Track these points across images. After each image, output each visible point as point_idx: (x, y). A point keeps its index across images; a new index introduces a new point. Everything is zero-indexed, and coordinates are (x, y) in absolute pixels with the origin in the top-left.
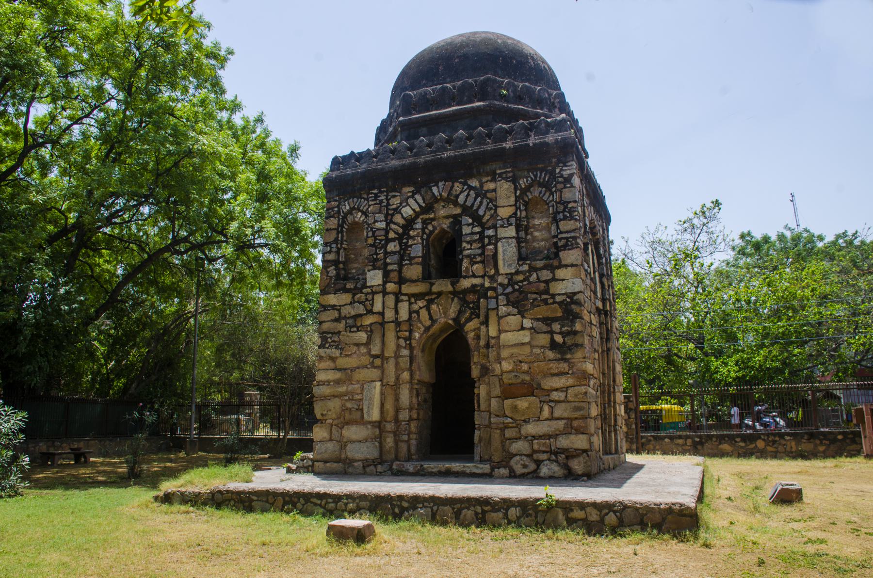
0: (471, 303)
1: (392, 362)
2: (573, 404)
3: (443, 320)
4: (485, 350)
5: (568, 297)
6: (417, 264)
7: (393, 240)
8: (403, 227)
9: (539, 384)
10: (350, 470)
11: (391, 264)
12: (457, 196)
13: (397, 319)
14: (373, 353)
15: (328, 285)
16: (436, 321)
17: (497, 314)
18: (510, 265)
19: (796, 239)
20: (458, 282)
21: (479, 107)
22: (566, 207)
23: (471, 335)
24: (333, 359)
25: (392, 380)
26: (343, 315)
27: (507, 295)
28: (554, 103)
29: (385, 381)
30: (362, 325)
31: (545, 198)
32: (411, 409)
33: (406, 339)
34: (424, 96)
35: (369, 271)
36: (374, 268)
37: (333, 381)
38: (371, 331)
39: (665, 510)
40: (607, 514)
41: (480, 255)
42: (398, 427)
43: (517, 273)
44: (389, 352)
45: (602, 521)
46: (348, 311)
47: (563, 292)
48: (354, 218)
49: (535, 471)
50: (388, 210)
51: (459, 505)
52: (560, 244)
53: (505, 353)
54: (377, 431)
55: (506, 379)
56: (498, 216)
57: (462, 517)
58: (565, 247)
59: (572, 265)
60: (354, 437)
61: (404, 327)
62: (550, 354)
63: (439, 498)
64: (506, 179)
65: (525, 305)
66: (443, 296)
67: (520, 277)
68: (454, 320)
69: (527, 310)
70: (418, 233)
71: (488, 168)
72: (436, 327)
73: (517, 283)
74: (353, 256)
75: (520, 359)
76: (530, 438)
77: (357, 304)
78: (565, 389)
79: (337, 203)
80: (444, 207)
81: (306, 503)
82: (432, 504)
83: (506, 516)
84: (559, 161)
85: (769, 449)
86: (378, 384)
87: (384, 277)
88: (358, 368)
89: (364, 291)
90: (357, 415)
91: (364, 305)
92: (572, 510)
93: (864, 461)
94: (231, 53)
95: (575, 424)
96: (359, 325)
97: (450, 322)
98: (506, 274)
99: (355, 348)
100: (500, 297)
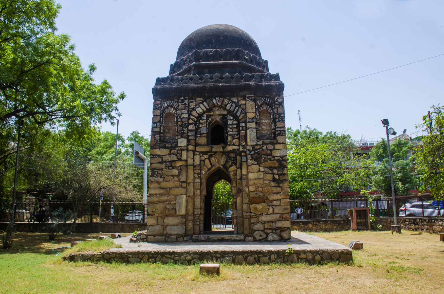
0: (232, 158)
1: (191, 185)
2: (283, 207)
3: (217, 165)
4: (240, 181)
6: (204, 137)
7: (192, 124)
8: (197, 118)
9: (267, 198)
10: (169, 240)
11: (191, 136)
12: (226, 105)
13: (194, 163)
14: (182, 180)
15: (155, 144)
16: (214, 165)
17: (247, 164)
18: (253, 141)
19: (311, 133)
20: (226, 147)
21: (236, 63)
22: (280, 116)
23: (232, 173)
24: (158, 183)
25: (192, 195)
26: (164, 160)
27: (252, 155)
28: (264, 65)
29: (188, 195)
31: (269, 111)
32: (201, 209)
33: (198, 174)
34: (206, 53)
35: (179, 138)
36: (182, 137)
37: (159, 194)
38: (181, 169)
39: (341, 252)
40: (316, 255)
41: (237, 135)
42: (194, 218)
43: (257, 145)
44: (190, 180)
45: (314, 258)
46: (167, 158)
47: (279, 155)
48: (170, 111)
49: (266, 238)
50: (189, 108)
51: (246, 255)
52: (277, 133)
53: (251, 183)
54: (184, 220)
55: (251, 195)
56: (247, 117)
57: (248, 260)
58: (279, 135)
60: (171, 223)
61: (198, 168)
62: (273, 184)
63: (236, 252)
64: (251, 100)
65: (260, 160)
66: (217, 154)
67: (258, 147)
68: (223, 165)
69: (261, 163)
70: (205, 122)
71: (242, 94)
72: (214, 168)
73: (256, 150)
74: (167, 130)
75: (258, 185)
76: (263, 223)
77: (172, 155)
78: (280, 200)
79: (160, 102)
80: (218, 110)
81: (162, 257)
82: (232, 255)
83: (270, 259)
84: (277, 94)
85: (314, 228)
86: (185, 196)
87: (187, 142)
88: (173, 188)
89: (176, 148)
90: (173, 212)
92: (300, 254)
93: (353, 232)
94: (59, 7)
95: (284, 216)
96: (174, 165)
97: (221, 167)
99: (172, 178)
100: (248, 156)
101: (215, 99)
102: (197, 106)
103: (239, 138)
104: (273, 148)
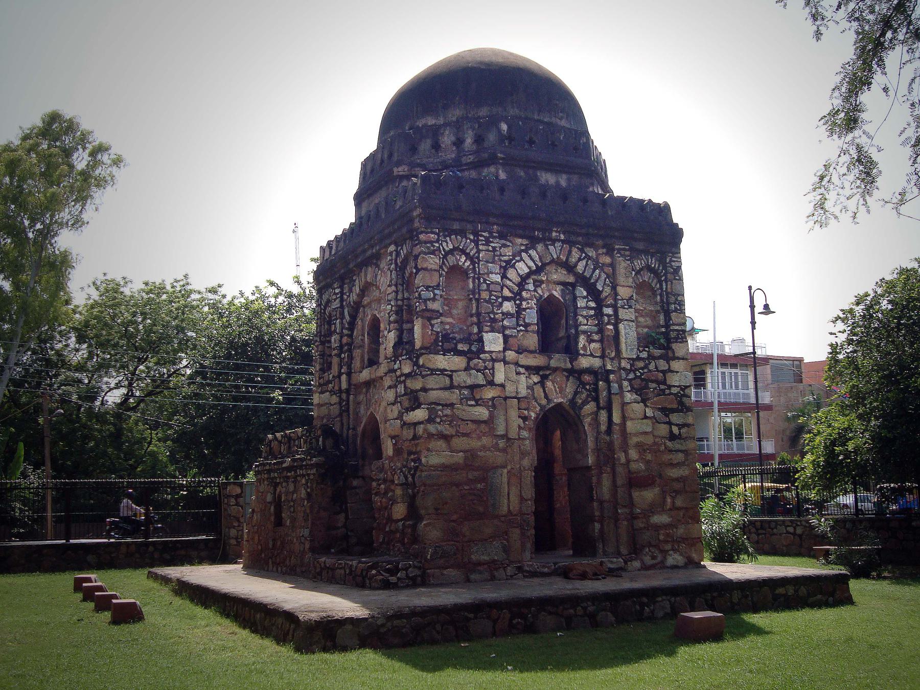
5: (682, 389)
6: (533, 332)
20: (576, 359)
27: (630, 381)
30: (481, 399)
38: (494, 406)
41: (597, 333)
43: (639, 358)
46: (462, 378)
65: (647, 393)
91: (483, 374)
98: (629, 359)
101: (553, 245)
103: (601, 341)
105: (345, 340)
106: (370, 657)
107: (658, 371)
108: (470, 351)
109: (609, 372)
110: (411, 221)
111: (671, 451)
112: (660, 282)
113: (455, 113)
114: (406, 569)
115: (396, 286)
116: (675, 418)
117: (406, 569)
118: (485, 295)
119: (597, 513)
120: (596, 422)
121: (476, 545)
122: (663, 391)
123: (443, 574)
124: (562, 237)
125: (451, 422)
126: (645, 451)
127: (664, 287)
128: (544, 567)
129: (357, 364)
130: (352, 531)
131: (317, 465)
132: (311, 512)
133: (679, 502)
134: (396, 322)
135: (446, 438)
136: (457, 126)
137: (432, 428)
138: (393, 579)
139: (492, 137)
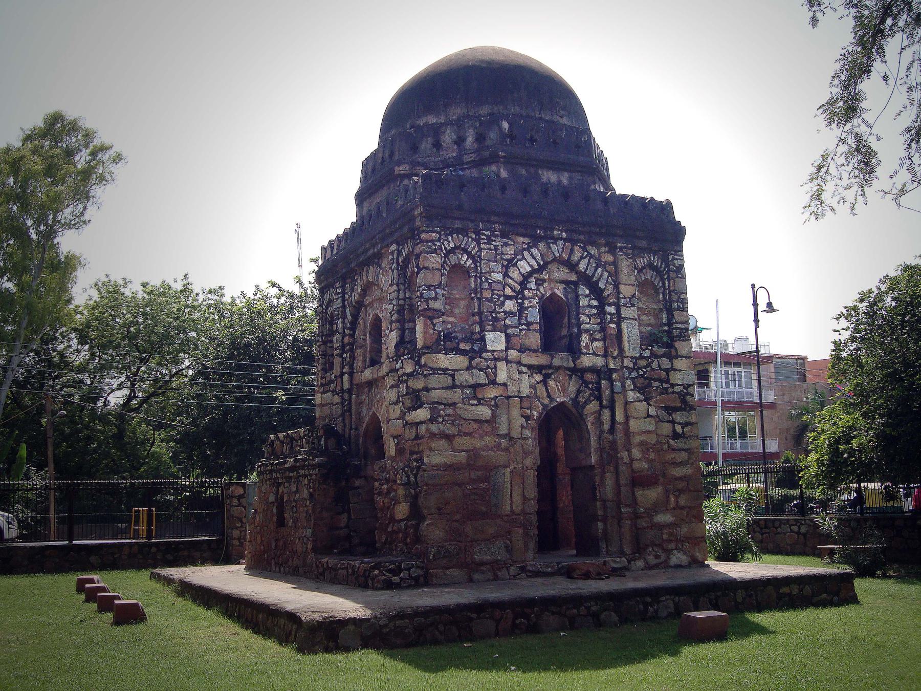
5: (685, 388)
6: (535, 330)
20: (579, 358)
23: (590, 419)
30: (483, 398)
38: (496, 405)
41: (599, 332)
43: (641, 357)
46: (464, 377)
59: (686, 357)
67: (644, 363)
77: (475, 371)
89: (484, 355)
102: (519, 257)
103: (604, 339)
104: (669, 366)
105: (347, 340)
106: (372, 657)
107: (661, 369)
108: (472, 350)
109: (611, 371)
110: (413, 219)
111: (674, 450)
112: (663, 280)
113: (456, 112)
114: (409, 569)
115: (398, 285)
116: (678, 417)
117: (409, 569)
118: (487, 294)
119: (600, 513)
120: (599, 421)
121: (479, 545)
122: (667, 389)
123: (445, 574)
124: (564, 235)
125: (453, 421)
126: (648, 450)
127: (667, 285)
128: (547, 566)
129: (359, 363)
130: (355, 531)
131: (319, 465)
132: (314, 512)
133: (682, 502)
134: (398, 321)
135: (449, 438)
136: (458, 124)
137: (434, 428)
138: (396, 579)
139: (493, 136)
